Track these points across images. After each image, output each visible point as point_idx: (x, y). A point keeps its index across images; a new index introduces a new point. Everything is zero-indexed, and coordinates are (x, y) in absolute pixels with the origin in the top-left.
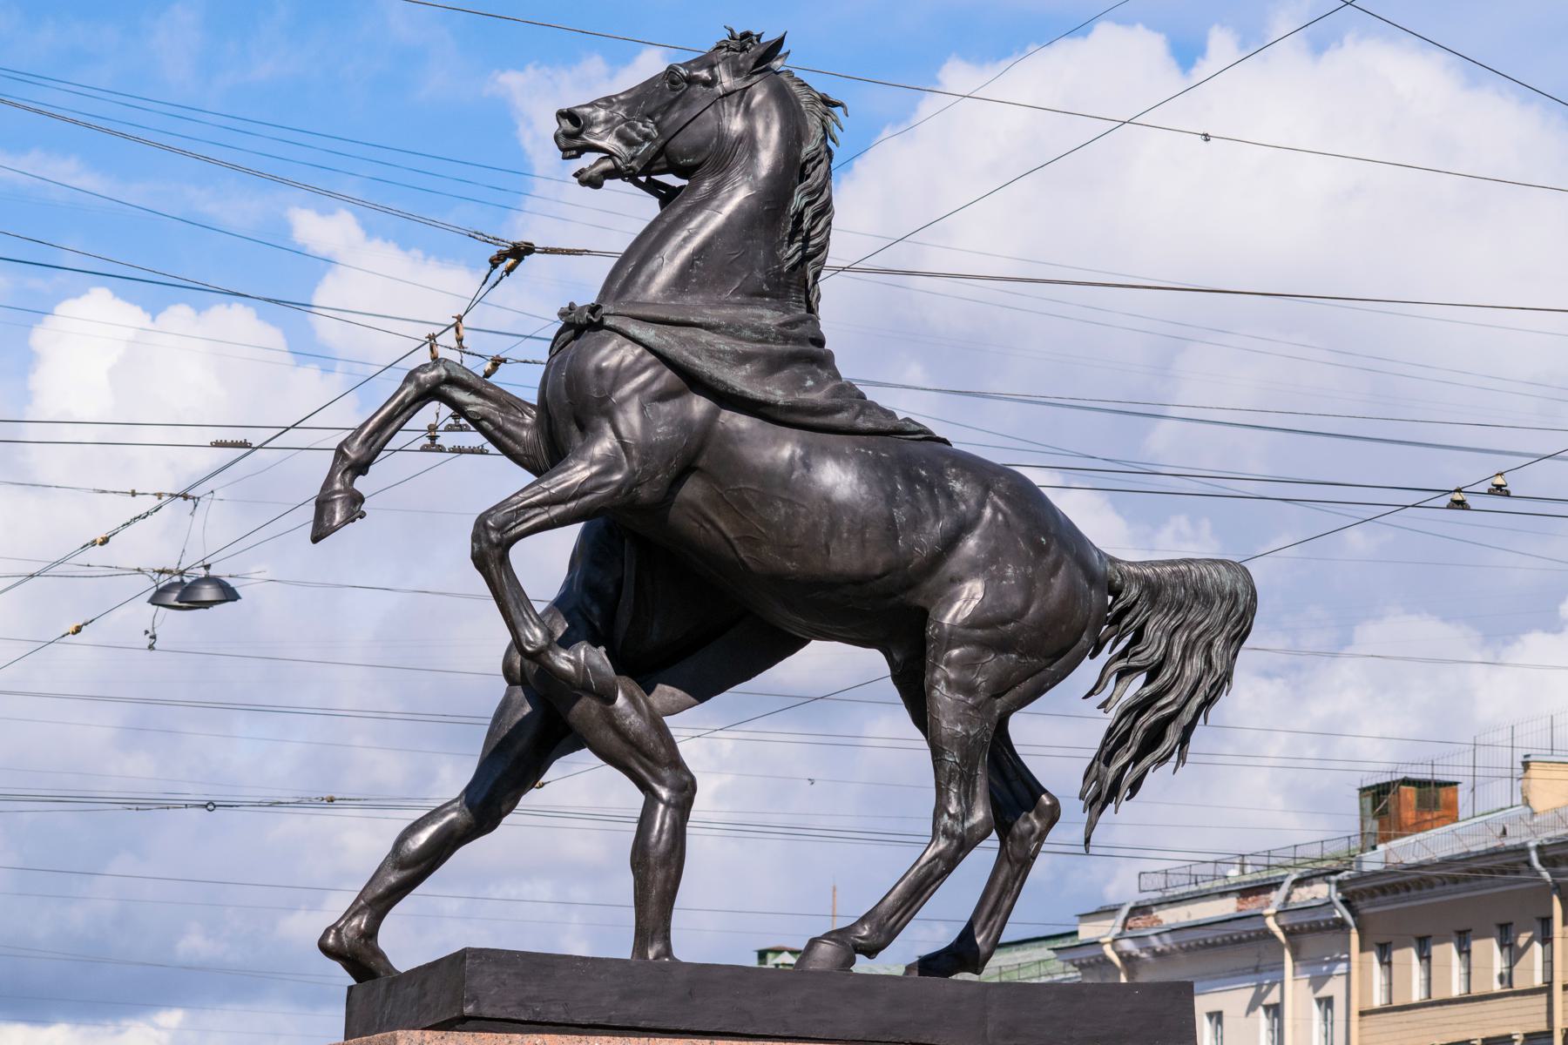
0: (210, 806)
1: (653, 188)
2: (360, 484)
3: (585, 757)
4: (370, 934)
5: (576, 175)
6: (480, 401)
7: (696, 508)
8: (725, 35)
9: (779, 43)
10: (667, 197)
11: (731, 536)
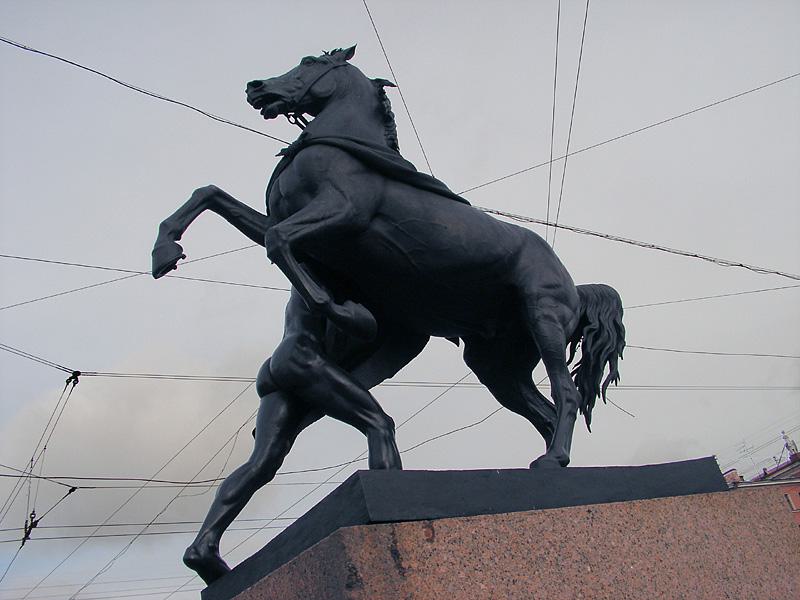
3: (327, 421)
4: (214, 549)
7: (384, 238)
9: (352, 50)
11: (405, 251)
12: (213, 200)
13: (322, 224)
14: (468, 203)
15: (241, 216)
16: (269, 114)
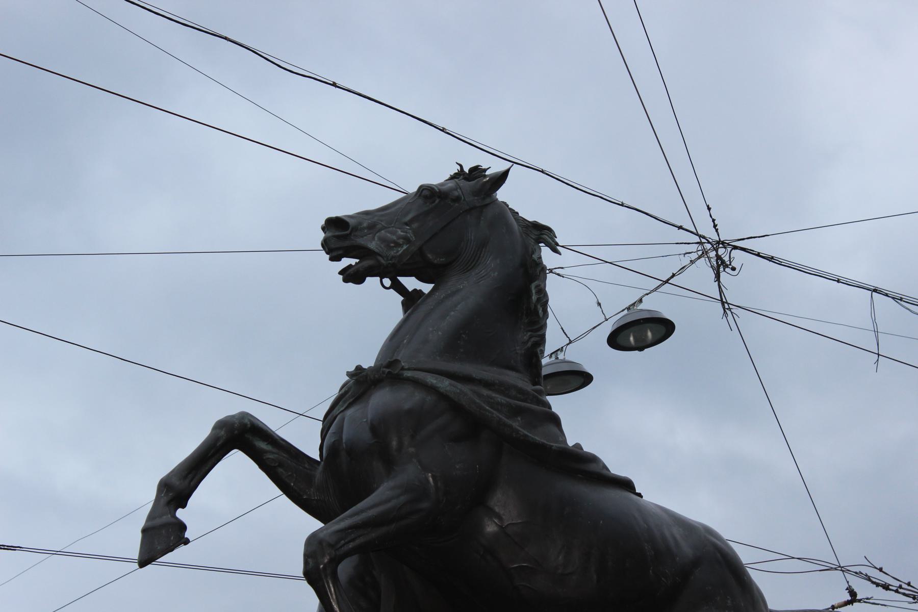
0: (709, 209)
1: (398, 287)
2: (180, 514)
5: (340, 273)
6: (275, 450)
8: (455, 169)
10: (411, 299)
12: (240, 435)
13: (383, 530)
14: (627, 485)
15: (281, 465)
16: (352, 276)
